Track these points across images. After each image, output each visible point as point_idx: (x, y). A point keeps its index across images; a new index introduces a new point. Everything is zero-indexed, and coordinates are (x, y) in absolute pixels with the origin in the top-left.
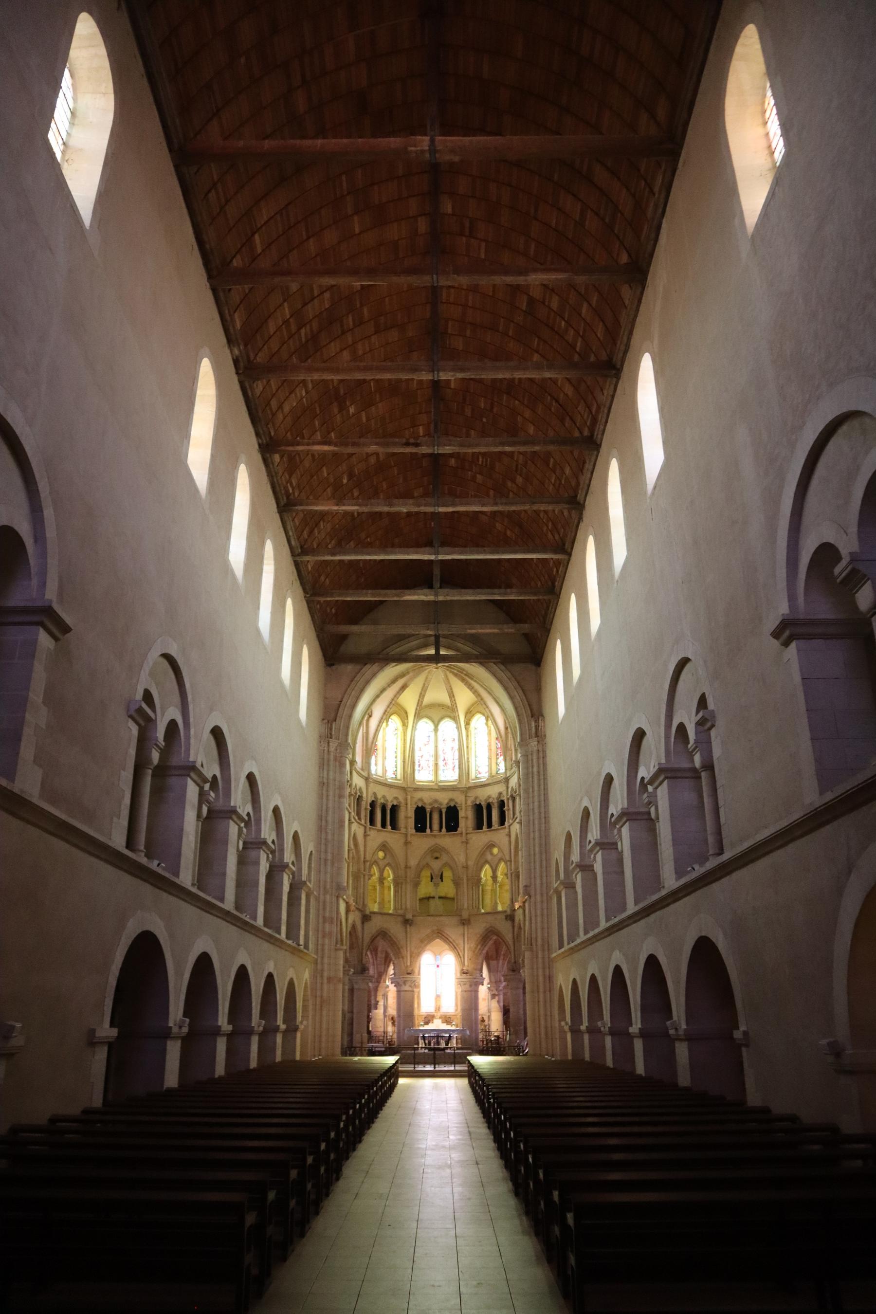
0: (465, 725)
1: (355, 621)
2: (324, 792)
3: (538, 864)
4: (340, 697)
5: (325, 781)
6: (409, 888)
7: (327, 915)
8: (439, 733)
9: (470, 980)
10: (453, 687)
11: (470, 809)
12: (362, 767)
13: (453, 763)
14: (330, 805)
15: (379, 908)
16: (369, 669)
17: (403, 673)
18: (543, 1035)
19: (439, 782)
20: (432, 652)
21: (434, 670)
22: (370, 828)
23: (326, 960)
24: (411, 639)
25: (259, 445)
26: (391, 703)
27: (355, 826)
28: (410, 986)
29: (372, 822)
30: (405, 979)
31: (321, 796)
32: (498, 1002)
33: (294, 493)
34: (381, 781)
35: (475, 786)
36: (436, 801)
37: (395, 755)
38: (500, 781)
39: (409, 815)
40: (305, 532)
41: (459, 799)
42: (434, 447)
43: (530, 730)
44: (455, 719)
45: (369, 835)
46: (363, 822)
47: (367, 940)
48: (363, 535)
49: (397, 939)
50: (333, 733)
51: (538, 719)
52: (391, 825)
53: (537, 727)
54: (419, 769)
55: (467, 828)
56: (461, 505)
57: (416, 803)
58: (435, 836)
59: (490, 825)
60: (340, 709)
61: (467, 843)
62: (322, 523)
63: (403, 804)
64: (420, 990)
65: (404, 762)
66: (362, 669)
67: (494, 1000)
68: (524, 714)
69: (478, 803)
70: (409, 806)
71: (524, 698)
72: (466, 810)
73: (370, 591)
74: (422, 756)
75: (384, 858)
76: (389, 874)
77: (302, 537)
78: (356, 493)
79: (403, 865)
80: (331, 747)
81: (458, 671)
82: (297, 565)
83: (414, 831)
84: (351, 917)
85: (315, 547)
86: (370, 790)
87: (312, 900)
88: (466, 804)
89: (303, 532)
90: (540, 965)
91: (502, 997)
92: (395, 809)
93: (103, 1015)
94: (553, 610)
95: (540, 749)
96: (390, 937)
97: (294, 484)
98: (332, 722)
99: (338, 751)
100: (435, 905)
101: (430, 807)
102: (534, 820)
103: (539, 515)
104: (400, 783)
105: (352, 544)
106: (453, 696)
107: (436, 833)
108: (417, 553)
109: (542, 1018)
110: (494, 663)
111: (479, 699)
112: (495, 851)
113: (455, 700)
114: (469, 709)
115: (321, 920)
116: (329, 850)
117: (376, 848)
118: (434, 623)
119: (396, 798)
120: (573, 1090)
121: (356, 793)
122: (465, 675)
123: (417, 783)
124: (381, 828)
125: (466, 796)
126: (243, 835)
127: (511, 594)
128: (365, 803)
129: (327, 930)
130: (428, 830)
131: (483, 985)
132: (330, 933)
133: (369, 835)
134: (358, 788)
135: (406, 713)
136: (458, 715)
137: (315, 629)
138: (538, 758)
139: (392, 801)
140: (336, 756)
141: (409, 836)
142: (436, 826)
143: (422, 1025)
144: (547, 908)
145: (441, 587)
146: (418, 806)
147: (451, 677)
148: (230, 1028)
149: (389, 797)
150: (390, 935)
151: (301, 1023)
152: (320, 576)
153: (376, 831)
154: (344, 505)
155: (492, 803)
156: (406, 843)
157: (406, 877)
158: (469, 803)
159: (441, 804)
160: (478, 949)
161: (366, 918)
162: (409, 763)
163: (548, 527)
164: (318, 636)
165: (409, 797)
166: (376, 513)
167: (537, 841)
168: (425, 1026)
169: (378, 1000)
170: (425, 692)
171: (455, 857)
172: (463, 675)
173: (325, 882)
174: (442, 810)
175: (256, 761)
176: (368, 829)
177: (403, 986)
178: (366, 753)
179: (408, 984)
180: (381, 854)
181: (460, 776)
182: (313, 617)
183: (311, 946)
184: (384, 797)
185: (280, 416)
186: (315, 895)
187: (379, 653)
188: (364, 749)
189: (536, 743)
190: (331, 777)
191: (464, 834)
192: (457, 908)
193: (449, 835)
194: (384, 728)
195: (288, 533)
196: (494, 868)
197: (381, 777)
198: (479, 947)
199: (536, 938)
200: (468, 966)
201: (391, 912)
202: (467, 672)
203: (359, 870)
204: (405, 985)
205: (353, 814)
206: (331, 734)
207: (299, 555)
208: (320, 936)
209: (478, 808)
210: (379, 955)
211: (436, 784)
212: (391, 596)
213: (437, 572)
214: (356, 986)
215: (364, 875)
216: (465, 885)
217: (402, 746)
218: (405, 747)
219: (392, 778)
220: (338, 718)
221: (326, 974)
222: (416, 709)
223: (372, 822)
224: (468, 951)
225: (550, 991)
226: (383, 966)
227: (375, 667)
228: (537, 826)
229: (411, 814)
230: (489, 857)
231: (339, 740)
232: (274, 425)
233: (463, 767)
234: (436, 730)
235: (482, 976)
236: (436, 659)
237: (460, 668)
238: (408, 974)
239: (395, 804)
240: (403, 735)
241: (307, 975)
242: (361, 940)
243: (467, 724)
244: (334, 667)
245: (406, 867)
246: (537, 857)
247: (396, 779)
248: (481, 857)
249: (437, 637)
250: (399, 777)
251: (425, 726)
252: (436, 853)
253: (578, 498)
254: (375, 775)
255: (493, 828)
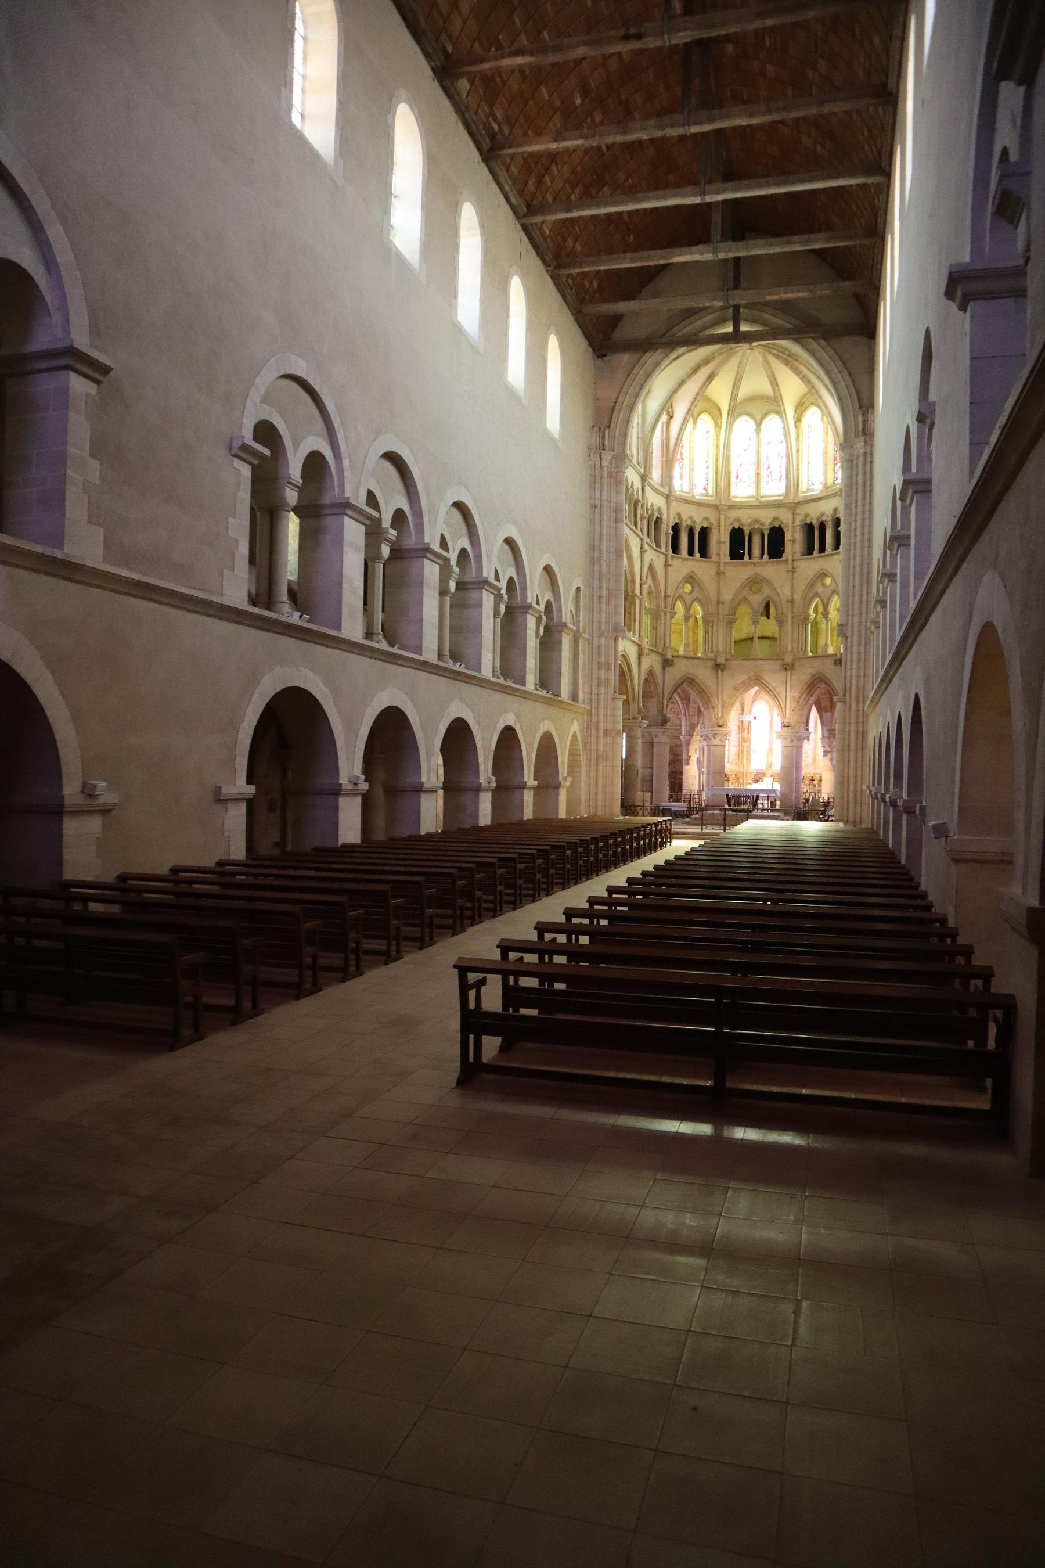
0: (795, 423)
1: (629, 295)
2: (597, 517)
3: (857, 599)
4: (615, 396)
5: (597, 502)
6: (722, 628)
7: (603, 660)
8: (762, 434)
9: (791, 734)
10: (775, 372)
11: (798, 529)
12: (662, 481)
13: (780, 472)
14: (605, 531)
15: (685, 651)
16: (650, 358)
17: (707, 358)
18: (851, 800)
19: (761, 497)
20: (729, 329)
21: (749, 351)
22: (672, 556)
23: (602, 711)
24: (702, 313)
25: (433, 70)
26: (695, 398)
27: (650, 555)
28: (721, 740)
29: (675, 549)
30: (715, 732)
31: (592, 522)
32: (831, 760)
33: (501, 130)
34: (688, 499)
35: (805, 501)
36: (757, 521)
37: (706, 465)
38: (836, 493)
39: (723, 539)
40: (530, 182)
41: (785, 518)
42: (663, 35)
43: (856, 426)
44: (780, 413)
45: (670, 565)
46: (663, 549)
47: (668, 689)
48: (621, 176)
49: (703, 684)
50: (606, 443)
51: (868, 411)
52: (699, 552)
53: (865, 422)
54: (736, 481)
55: (793, 554)
56: (722, 118)
57: (731, 524)
58: (754, 564)
59: (822, 549)
60: (615, 414)
61: (793, 572)
62: (554, 167)
63: (715, 526)
64: (750, 745)
65: (717, 473)
66: (641, 358)
67: (826, 757)
68: (850, 406)
69: (808, 522)
70: (722, 528)
71: (851, 384)
72: (794, 531)
73: (628, 255)
74: (740, 465)
75: (692, 592)
76: (698, 611)
77: (526, 191)
78: (598, 119)
79: (714, 599)
80: (604, 461)
81: (778, 351)
82: (525, 228)
83: (729, 558)
84: (646, 663)
85: (550, 201)
86: (671, 510)
87: (582, 646)
88: (793, 523)
89: (527, 182)
90: (853, 720)
91: (835, 754)
92: (704, 532)
93: (956, 754)
94: (879, 259)
95: (868, 450)
96: (698, 684)
97: (499, 116)
98: (604, 429)
99: (613, 465)
100: (760, 648)
101: (749, 528)
102: (855, 543)
103: (851, 118)
104: (711, 499)
105: (606, 189)
106: (777, 384)
107: (755, 560)
108: (676, 196)
109: (852, 780)
110: (813, 338)
111: (810, 386)
112: (828, 581)
113: (779, 390)
114: (800, 401)
115: (595, 666)
116: (604, 585)
117: (680, 580)
118: (723, 290)
119: (706, 519)
120: (366, 855)
121: (652, 515)
122: (789, 355)
123: (733, 499)
124: (687, 556)
125: (793, 514)
126: (453, 574)
127: (816, 240)
128: (665, 527)
129: (603, 676)
130: (746, 557)
131: (808, 740)
132: (607, 681)
133: (670, 565)
134: (655, 508)
135: (720, 410)
136: (784, 410)
137: (571, 312)
138: (865, 464)
139: (701, 523)
140: (611, 471)
141: (722, 563)
142: (756, 552)
143: (749, 783)
144: (865, 652)
145: (721, 241)
146: (734, 528)
147: (772, 359)
148: (536, 783)
149: (698, 518)
150: (699, 682)
151: (565, 779)
152: (565, 240)
153: (680, 560)
154: (564, 140)
155: (825, 521)
156: (719, 573)
157: (718, 614)
158: (798, 522)
159: (762, 524)
160: (802, 699)
161: (667, 663)
162: (724, 474)
163: (863, 135)
164: (576, 319)
165: (722, 517)
166: (634, 142)
167: (858, 568)
168: (754, 785)
169: (689, 754)
170: (740, 380)
171: (778, 590)
172: (785, 356)
173: (600, 623)
174: (764, 532)
175: (466, 487)
176: (669, 557)
177: (713, 739)
178: (667, 464)
179: (718, 738)
180: (688, 588)
181: (787, 488)
182: (564, 297)
183: (581, 696)
184: (691, 518)
185: (457, 23)
186: (586, 639)
187: (663, 336)
188: (664, 459)
189: (862, 444)
190: (605, 498)
191: (790, 562)
192: (780, 649)
193: (772, 562)
194: (691, 432)
195: (503, 187)
196: (825, 601)
197: (687, 493)
198: (804, 696)
199: (850, 688)
200: (790, 718)
201: (699, 655)
202: (790, 352)
203: (658, 607)
204: (715, 739)
205: (646, 539)
206: (603, 444)
207: (525, 216)
208: (595, 683)
209: (809, 528)
210: (691, 704)
211: (758, 499)
212: (654, 259)
213: (717, 218)
214: (655, 740)
215: (665, 614)
216: (790, 623)
217: (715, 453)
218: (717, 455)
219: (702, 495)
220: (612, 424)
221: (601, 726)
222: (730, 405)
223: (675, 549)
224: (790, 701)
225: (862, 750)
226: (696, 717)
227: (659, 354)
228: (858, 551)
229: (726, 538)
230: (820, 589)
231: (614, 451)
232: (450, 36)
233: (792, 480)
234: (758, 430)
235: (807, 730)
236: (737, 338)
237: (780, 347)
238: (719, 726)
239: (705, 526)
240: (715, 438)
241: (575, 727)
242: (661, 689)
243: (798, 420)
244: (607, 358)
245: (718, 602)
246: (857, 589)
247: (707, 495)
248: (810, 588)
249: (736, 308)
250: (710, 492)
251: (744, 425)
252: (755, 583)
253: (889, 86)
254: (679, 491)
255: (826, 553)
